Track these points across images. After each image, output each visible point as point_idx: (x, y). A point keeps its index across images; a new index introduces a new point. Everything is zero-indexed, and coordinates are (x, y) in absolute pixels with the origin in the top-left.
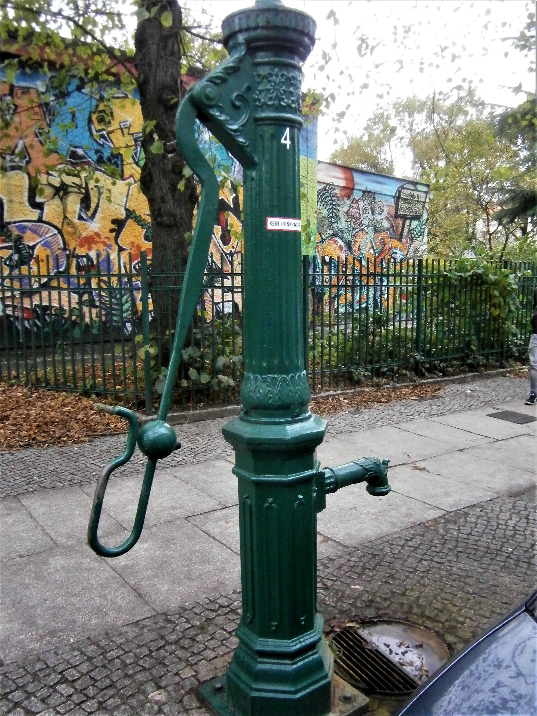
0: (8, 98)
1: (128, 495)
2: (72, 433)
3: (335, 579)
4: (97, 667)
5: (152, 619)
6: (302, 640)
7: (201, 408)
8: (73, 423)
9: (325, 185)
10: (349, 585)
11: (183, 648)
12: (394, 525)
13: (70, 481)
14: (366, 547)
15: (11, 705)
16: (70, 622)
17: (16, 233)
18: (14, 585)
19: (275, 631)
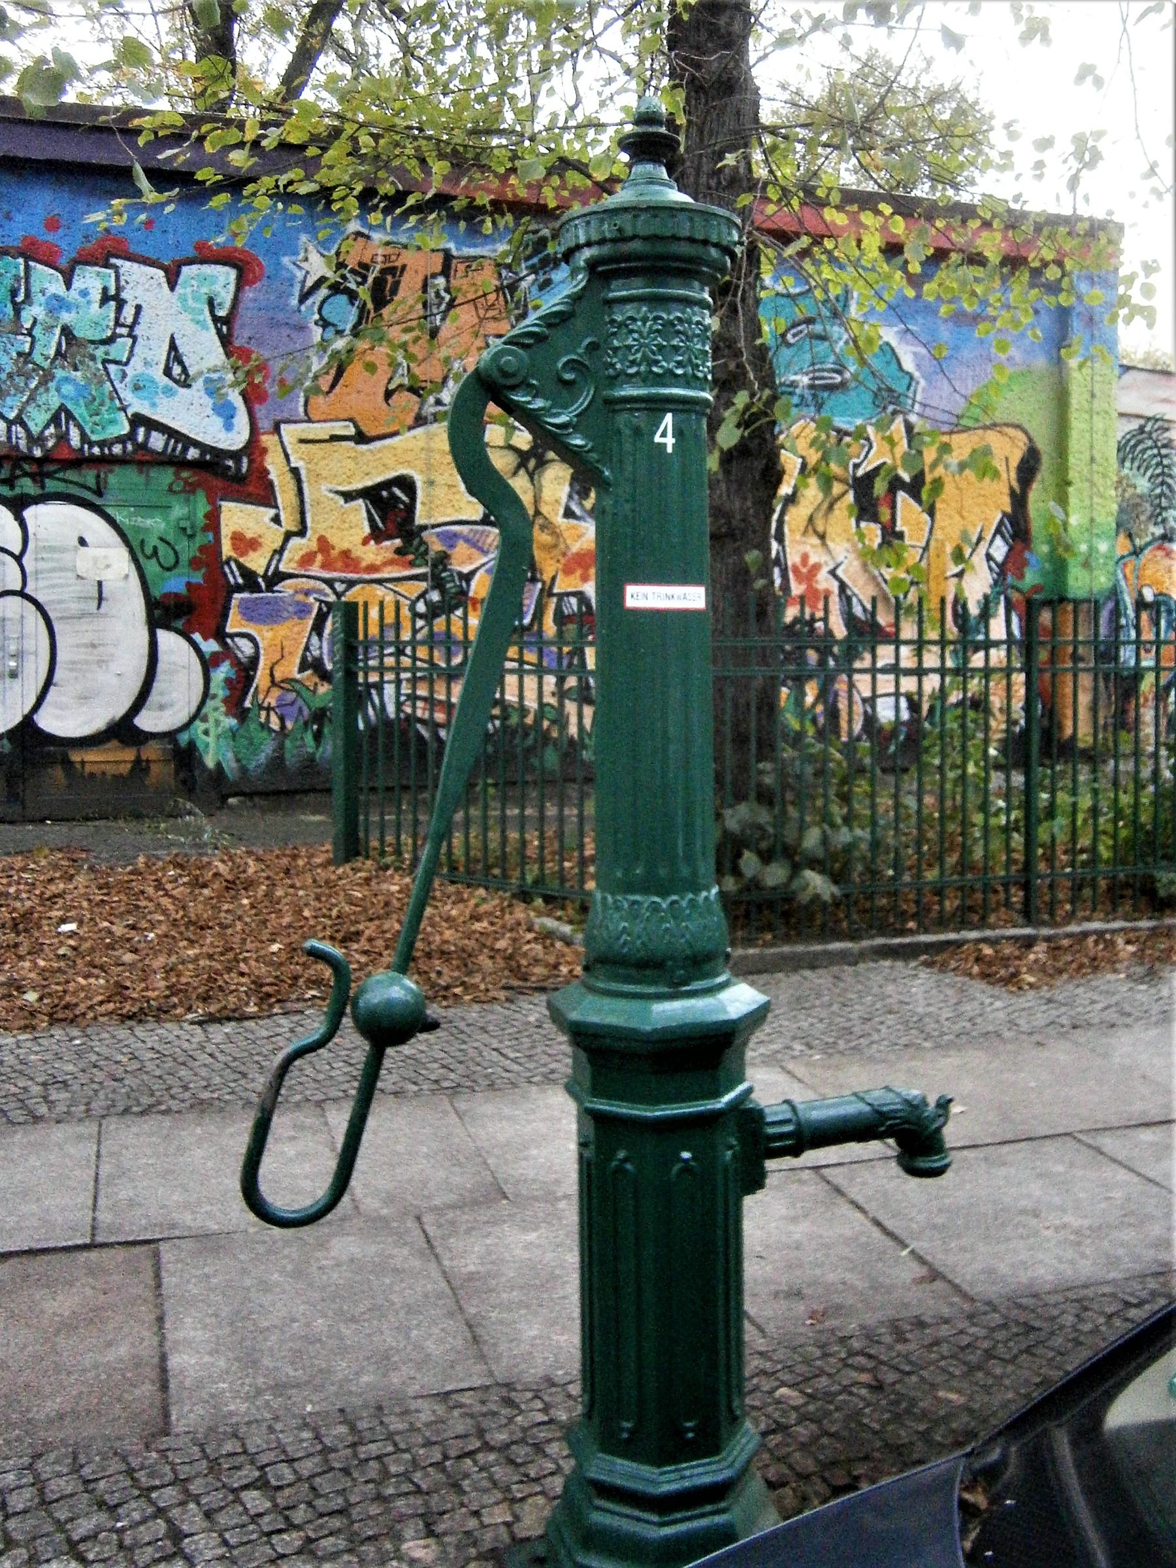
0: (441, 281)
1: (541, 1125)
2: (477, 979)
3: (907, 1368)
4: (332, 1469)
5: (480, 1394)
6: (687, 1473)
7: (766, 945)
8: (484, 960)
9: (1142, 422)
10: (934, 1386)
11: (512, 1462)
12: (1114, 1262)
13: (436, 1081)
14: (1020, 1306)
15: (150, 1510)
16: (321, 1371)
17: (436, 546)
18: (248, 1282)
19: (628, 1441)
